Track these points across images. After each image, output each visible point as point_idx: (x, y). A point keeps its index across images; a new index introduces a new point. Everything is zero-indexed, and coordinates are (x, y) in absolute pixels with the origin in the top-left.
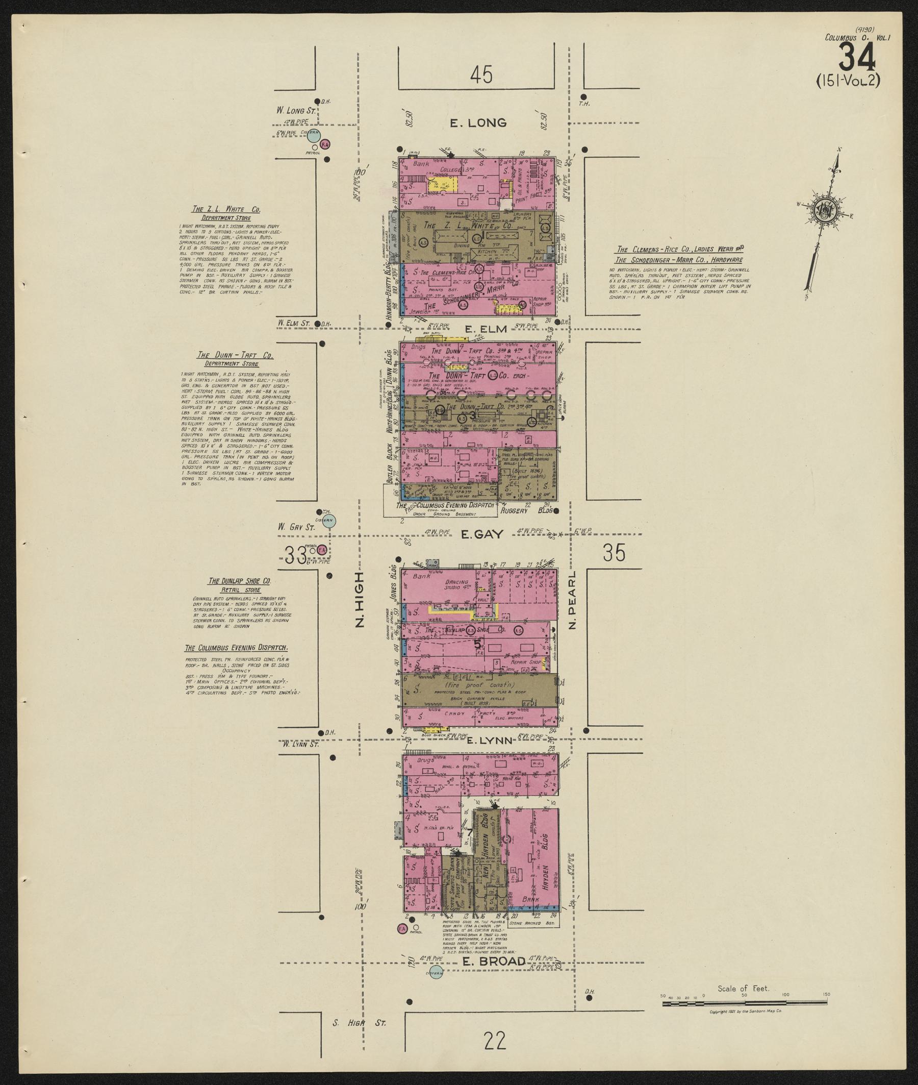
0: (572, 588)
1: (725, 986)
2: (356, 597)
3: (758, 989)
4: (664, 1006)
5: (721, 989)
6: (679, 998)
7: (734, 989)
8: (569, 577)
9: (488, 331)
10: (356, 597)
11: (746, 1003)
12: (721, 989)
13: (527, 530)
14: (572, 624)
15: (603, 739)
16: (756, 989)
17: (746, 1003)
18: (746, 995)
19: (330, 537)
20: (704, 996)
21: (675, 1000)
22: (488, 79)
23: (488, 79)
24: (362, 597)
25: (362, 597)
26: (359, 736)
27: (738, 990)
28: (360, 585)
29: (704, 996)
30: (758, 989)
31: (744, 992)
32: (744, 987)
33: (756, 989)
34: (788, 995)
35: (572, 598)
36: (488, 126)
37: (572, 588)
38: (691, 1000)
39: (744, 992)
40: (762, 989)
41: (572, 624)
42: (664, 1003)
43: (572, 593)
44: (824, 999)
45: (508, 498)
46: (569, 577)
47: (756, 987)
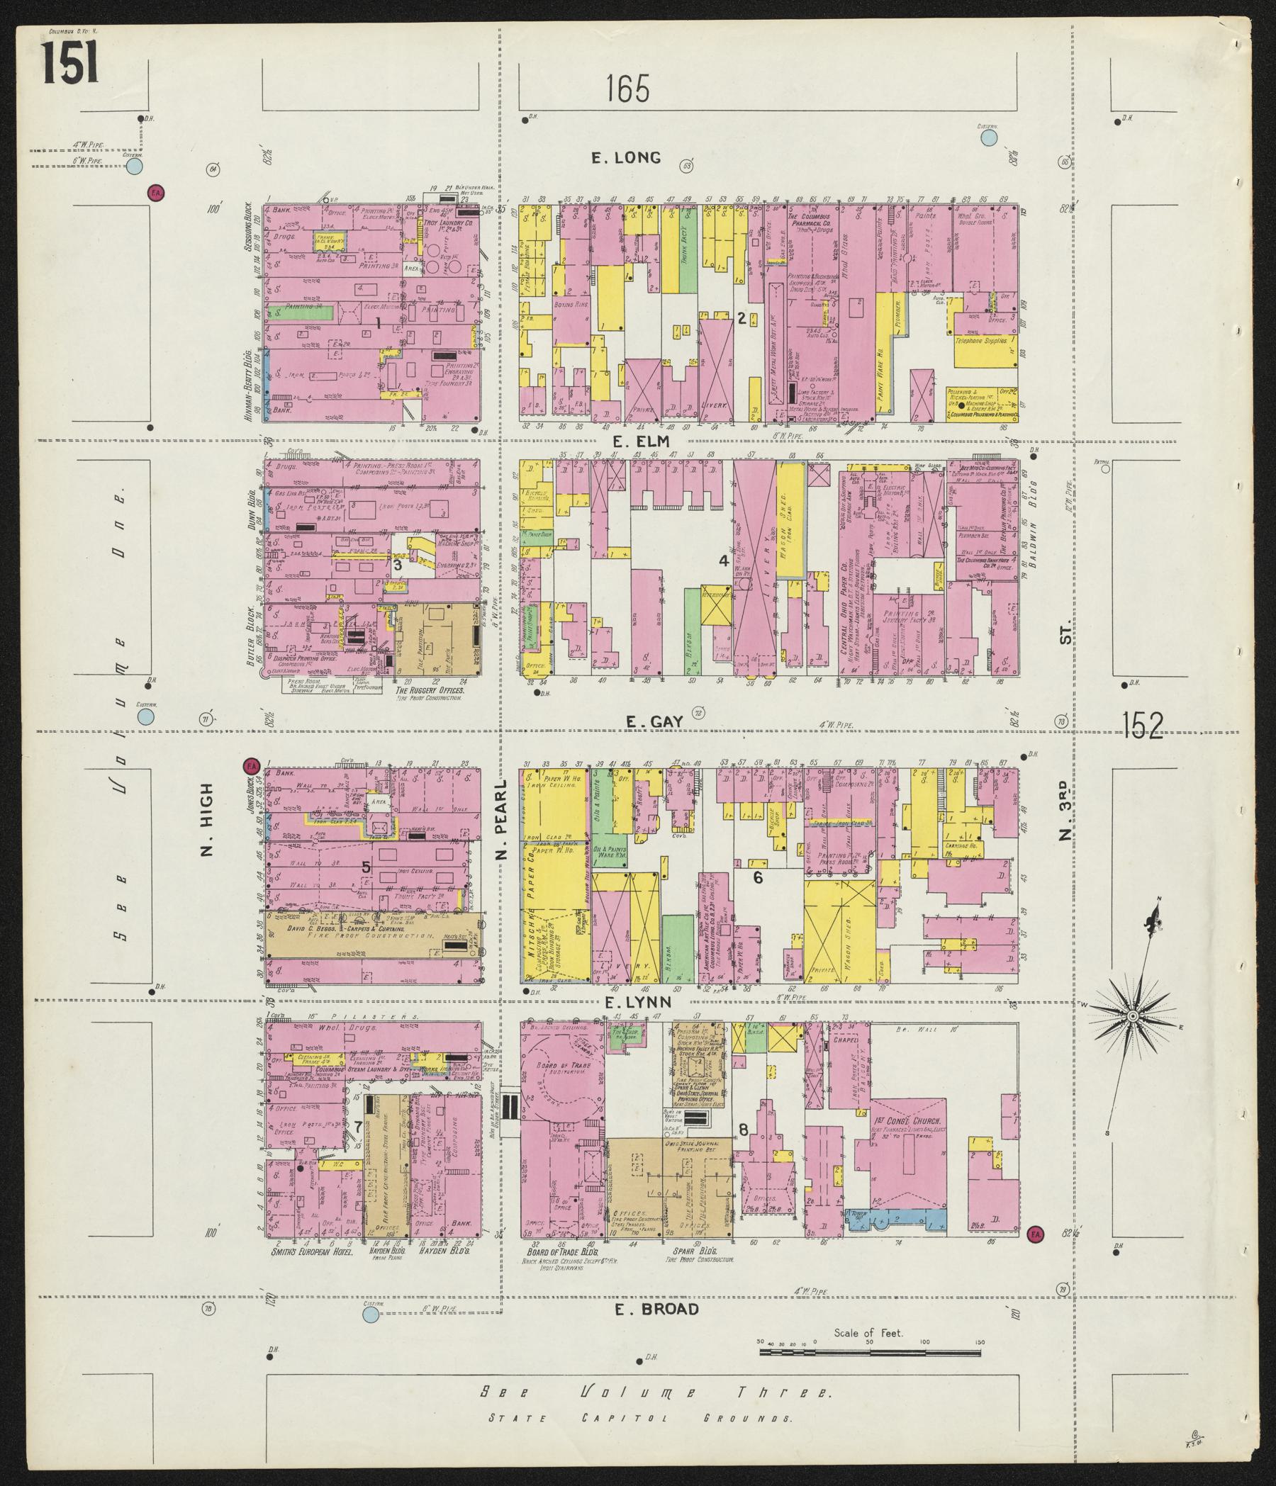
0: (501, 803)
1: (844, 1329)
2: (202, 812)
3: (888, 1334)
4: (761, 1355)
5: (838, 1334)
6: (782, 1344)
7: (856, 1334)
8: (496, 787)
9: (647, 444)
10: (202, 812)
11: (871, 1353)
12: (838, 1334)
13: (831, 724)
14: (204, 850)
15: (576, 1002)
16: (885, 1334)
17: (871, 1353)
18: (872, 1342)
19: (501, 731)
20: (815, 1342)
21: (776, 1347)
22: (643, 97)
23: (643, 97)
24: (210, 812)
25: (210, 812)
26: (808, 1002)
27: (861, 1334)
28: (208, 798)
29: (815, 1342)
30: (888, 1334)
31: (869, 1338)
32: (869, 1331)
33: (885, 1334)
34: (927, 1342)
35: (501, 816)
36: (640, 161)
37: (501, 803)
38: (798, 1347)
39: (869, 1338)
40: (894, 1334)
41: (204, 850)
42: (761, 1350)
43: (500, 809)
44: (976, 1348)
45: (1004, 673)
46: (496, 787)
47: (886, 1331)
